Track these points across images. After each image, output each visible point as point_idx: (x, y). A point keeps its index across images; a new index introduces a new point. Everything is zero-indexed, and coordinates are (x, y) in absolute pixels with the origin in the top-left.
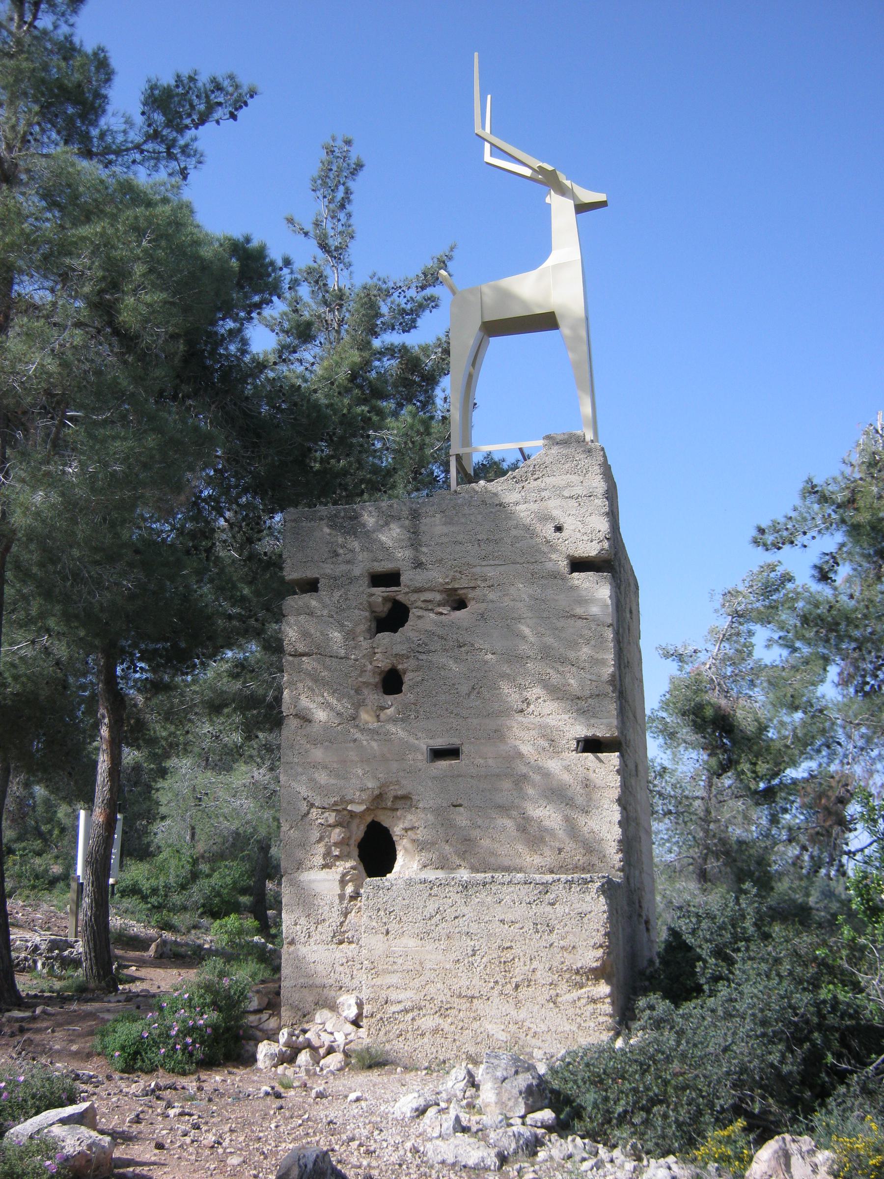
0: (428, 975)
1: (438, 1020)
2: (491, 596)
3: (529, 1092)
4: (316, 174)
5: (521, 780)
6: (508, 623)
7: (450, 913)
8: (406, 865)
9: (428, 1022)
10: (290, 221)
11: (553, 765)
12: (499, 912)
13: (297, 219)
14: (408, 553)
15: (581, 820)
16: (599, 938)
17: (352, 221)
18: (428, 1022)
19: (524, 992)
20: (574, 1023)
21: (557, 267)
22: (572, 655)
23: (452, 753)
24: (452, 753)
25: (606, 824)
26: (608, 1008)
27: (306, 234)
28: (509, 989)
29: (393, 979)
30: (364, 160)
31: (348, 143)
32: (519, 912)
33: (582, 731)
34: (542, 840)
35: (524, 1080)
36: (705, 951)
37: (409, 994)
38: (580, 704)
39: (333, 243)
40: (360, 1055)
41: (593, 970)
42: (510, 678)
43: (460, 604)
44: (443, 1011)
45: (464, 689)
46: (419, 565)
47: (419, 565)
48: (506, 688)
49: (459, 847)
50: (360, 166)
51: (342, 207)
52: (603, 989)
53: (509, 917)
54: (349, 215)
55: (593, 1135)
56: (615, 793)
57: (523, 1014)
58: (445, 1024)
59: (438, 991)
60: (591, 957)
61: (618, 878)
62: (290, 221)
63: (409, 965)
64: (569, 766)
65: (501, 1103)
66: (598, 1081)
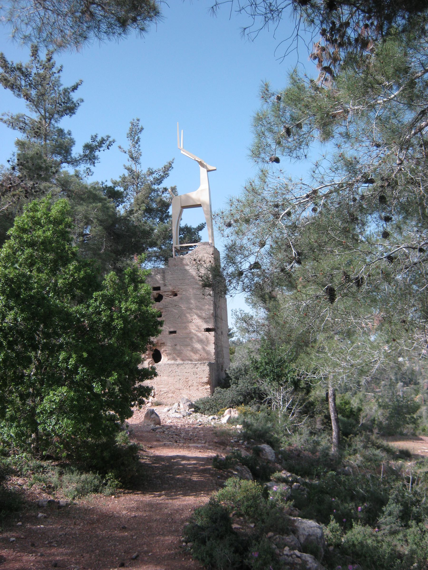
0: (170, 385)
1: (172, 394)
2: (184, 293)
3: (189, 405)
4: (128, 132)
5: (191, 339)
6: (188, 300)
7: (174, 371)
8: (164, 359)
9: (170, 395)
10: (120, 147)
11: (199, 334)
12: (185, 370)
13: (122, 147)
14: (162, 282)
15: (206, 347)
16: (207, 376)
17: (140, 148)
18: (170, 395)
19: (191, 388)
20: (202, 393)
21: (202, 190)
22: (203, 308)
23: (174, 332)
24: (174, 332)
25: (211, 348)
26: (209, 390)
27: (125, 152)
28: (188, 387)
29: (162, 386)
30: (144, 127)
31: (138, 120)
32: (190, 370)
33: (206, 326)
34: (197, 352)
35: (188, 403)
36: (233, 377)
37: (166, 389)
38: (205, 320)
39: (134, 156)
40: (155, 403)
41: (206, 382)
42: (189, 313)
43: (176, 295)
44: (173, 393)
45: (177, 317)
46: (165, 285)
47: (165, 285)
48: (188, 315)
49: (177, 354)
50: (142, 129)
51: (137, 143)
52: (209, 386)
53: (187, 371)
54: (139, 146)
55: (202, 413)
56: (213, 341)
57: (191, 392)
58: (174, 395)
59: (172, 388)
60: (206, 380)
61: (213, 361)
62: (120, 147)
63: (165, 383)
64: (204, 335)
65: (184, 408)
66: (203, 403)
